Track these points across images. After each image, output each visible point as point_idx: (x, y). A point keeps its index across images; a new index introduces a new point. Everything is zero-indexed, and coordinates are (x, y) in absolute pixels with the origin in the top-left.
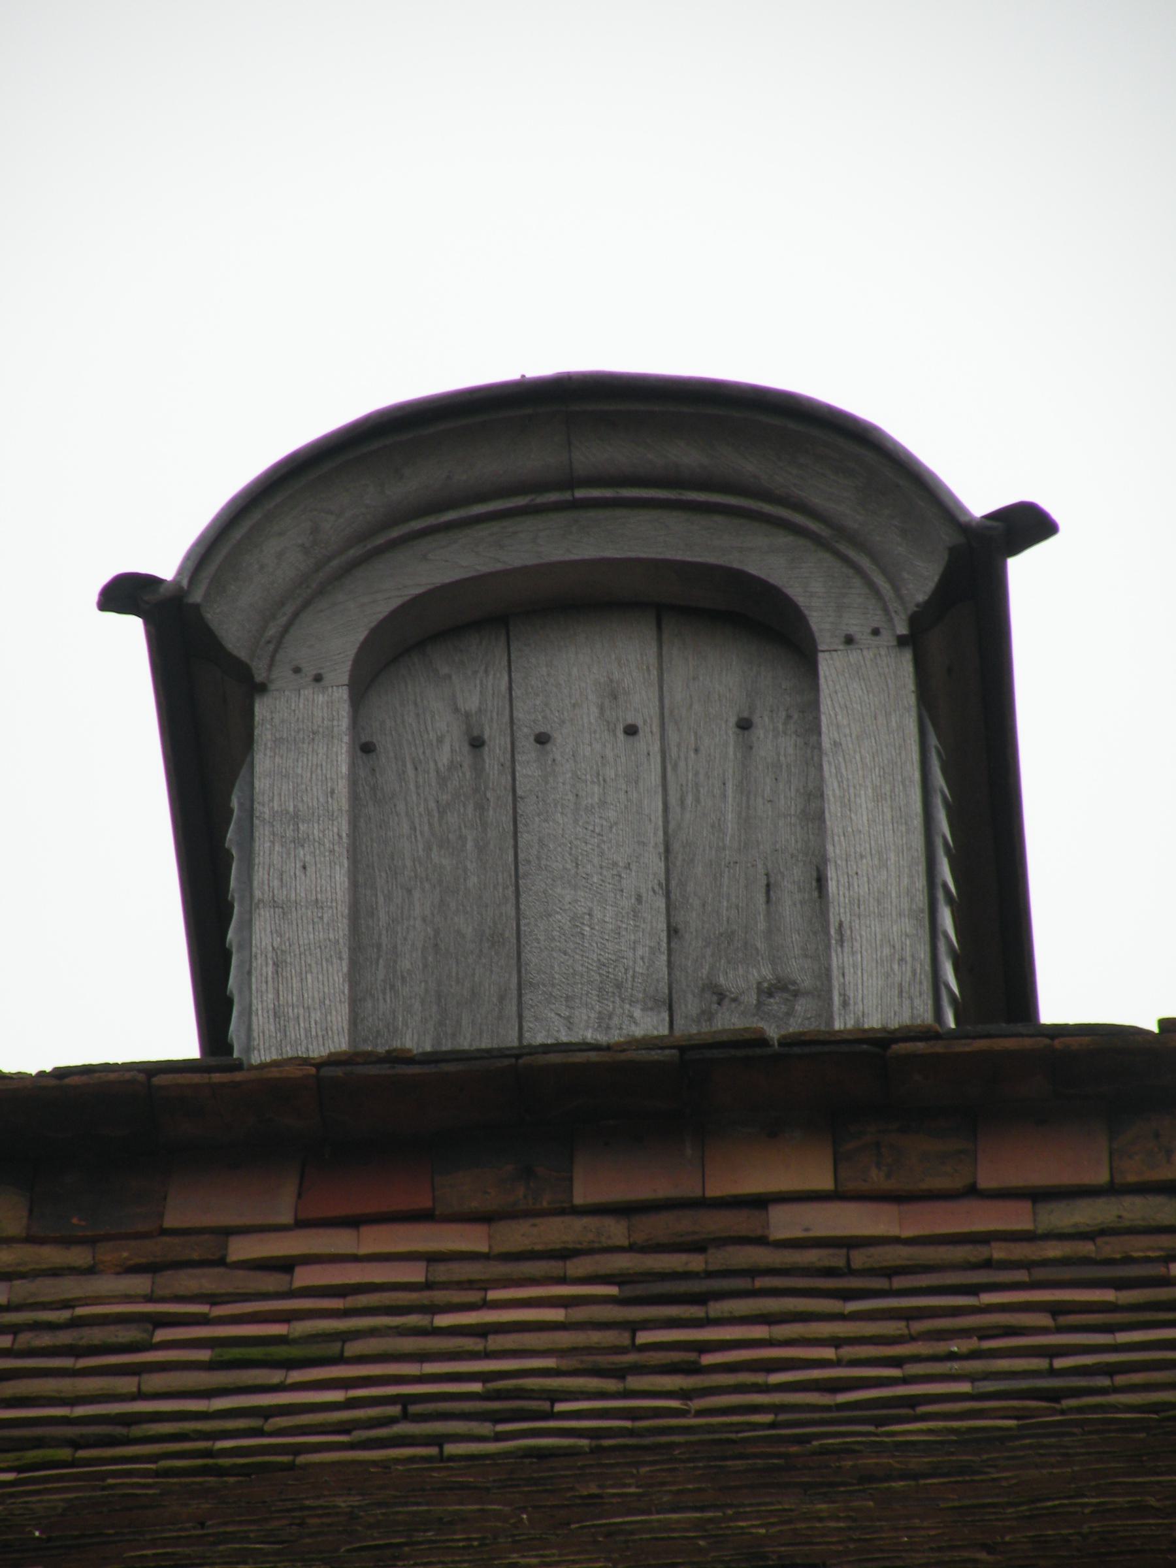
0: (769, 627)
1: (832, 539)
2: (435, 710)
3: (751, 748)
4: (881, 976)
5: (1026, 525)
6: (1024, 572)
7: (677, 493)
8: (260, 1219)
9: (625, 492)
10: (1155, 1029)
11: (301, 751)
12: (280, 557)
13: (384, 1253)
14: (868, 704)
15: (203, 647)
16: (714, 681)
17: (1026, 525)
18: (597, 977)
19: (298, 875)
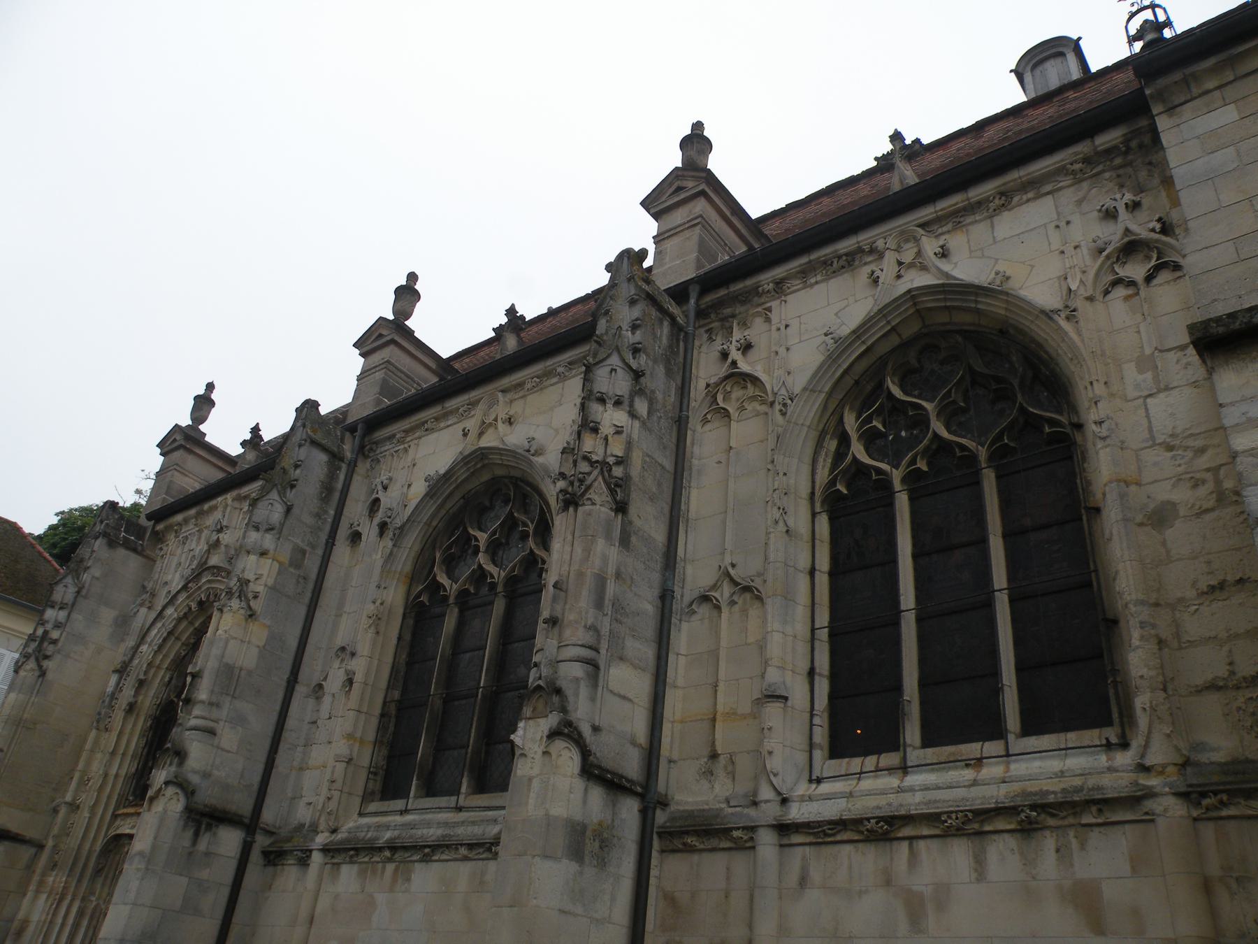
0: (1062, 54)
1: (1065, 46)
2: (1038, 71)
3: (651, 499)
4: (1076, 74)
5: (1080, 38)
6: (1081, 42)
7: (1053, 47)
8: (1030, 112)
9: (1048, 49)
10: (1014, 95)
11: (1028, 77)
12: (1023, 64)
13: (1040, 111)
14: (1071, 58)
15: (1019, 73)
16: (1059, 60)
17: (1080, 38)
18: (1054, 83)
19: (1030, 86)
